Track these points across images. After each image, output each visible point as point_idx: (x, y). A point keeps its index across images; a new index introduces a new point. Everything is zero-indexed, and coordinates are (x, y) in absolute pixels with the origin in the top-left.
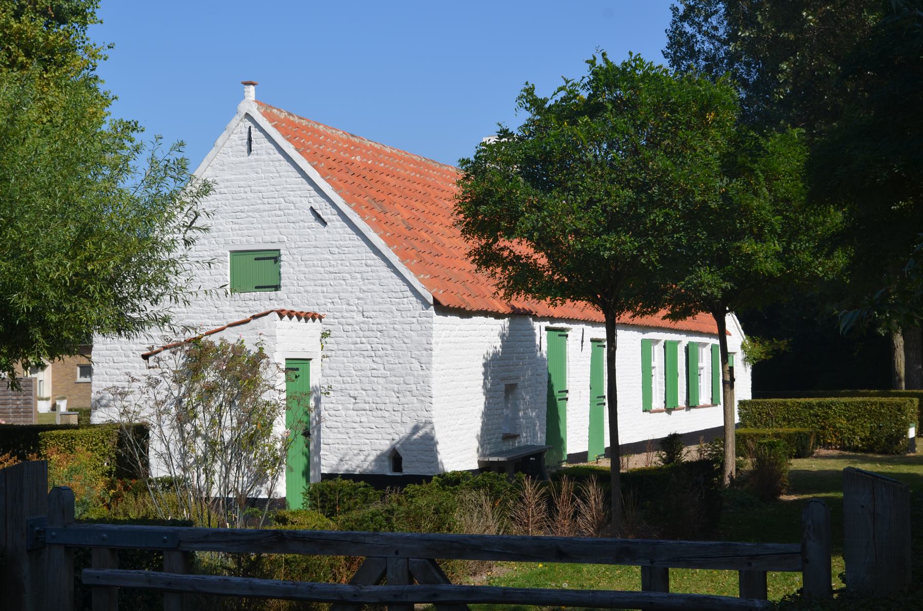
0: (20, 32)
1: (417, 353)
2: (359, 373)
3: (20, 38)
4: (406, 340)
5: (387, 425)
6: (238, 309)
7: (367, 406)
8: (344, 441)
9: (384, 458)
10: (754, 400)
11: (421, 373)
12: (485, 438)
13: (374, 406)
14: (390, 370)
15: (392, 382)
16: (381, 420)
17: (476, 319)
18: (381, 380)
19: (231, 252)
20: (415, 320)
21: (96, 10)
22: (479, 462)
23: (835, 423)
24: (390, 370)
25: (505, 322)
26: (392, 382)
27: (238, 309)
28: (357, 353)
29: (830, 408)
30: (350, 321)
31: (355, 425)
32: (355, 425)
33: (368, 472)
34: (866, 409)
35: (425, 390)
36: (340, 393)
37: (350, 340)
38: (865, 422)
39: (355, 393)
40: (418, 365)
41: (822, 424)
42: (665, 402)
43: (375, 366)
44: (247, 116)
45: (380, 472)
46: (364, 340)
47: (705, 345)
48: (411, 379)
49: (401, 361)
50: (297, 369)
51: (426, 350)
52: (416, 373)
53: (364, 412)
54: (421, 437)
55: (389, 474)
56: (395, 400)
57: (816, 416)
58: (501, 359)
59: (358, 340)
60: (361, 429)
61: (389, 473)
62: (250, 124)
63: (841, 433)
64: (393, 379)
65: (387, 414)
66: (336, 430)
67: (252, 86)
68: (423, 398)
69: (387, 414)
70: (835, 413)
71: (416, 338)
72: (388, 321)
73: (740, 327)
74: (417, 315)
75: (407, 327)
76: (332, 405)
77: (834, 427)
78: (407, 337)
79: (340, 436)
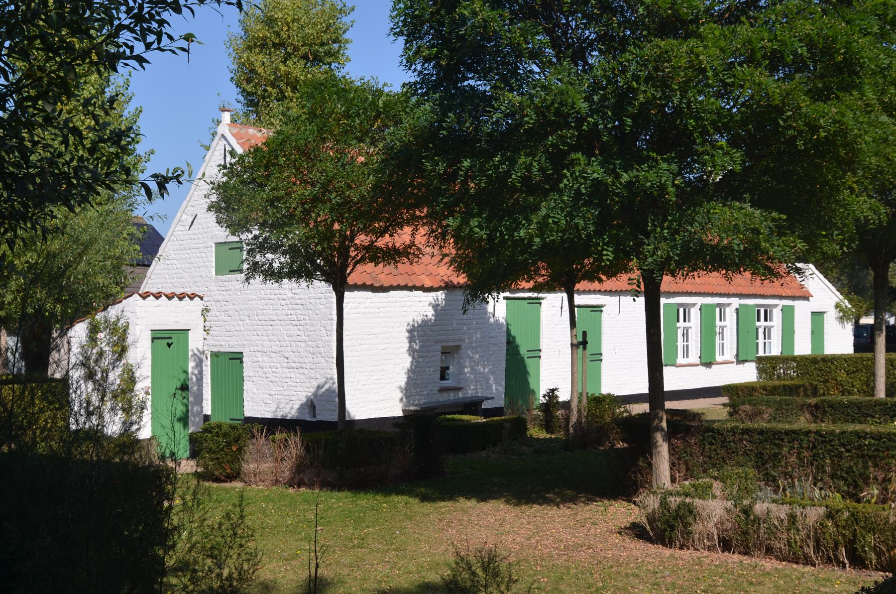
0: (287, 74)
1: (324, 322)
2: (289, 339)
3: (288, 78)
4: (317, 312)
5: (307, 380)
6: (219, 288)
7: (294, 365)
8: (280, 393)
9: (305, 407)
10: (859, 355)
11: (327, 338)
12: (409, 390)
13: (298, 364)
14: (308, 336)
15: (309, 346)
16: (302, 376)
17: (392, 293)
18: (303, 344)
19: (216, 244)
20: (322, 296)
21: (345, 51)
22: (403, 411)
23: (836, 376)
24: (308, 336)
25: (441, 295)
26: (309, 346)
27: (219, 288)
28: (288, 322)
29: (832, 363)
30: (284, 297)
31: (287, 380)
32: (287, 380)
33: (295, 418)
34: (863, 364)
35: (329, 352)
36: (278, 355)
37: (284, 312)
38: (862, 376)
39: (286, 354)
40: (324, 332)
41: (826, 377)
42: (700, 357)
43: (299, 333)
44: (223, 136)
45: (302, 418)
46: (293, 312)
47: (776, 306)
48: (320, 343)
49: (314, 329)
50: (170, 338)
51: (329, 320)
52: (323, 338)
53: (292, 370)
54: (327, 390)
55: (309, 419)
56: (311, 360)
57: (820, 370)
58: (434, 325)
59: (289, 312)
60: (291, 383)
61: (308, 418)
62: (225, 142)
63: (842, 385)
64: (310, 343)
65: (306, 372)
66: (276, 384)
67: (226, 113)
68: (328, 359)
69: (306, 372)
70: (837, 368)
71: (323, 310)
72: (306, 296)
73: (834, 289)
74: (324, 292)
75: (318, 301)
76: (274, 364)
77: (836, 380)
78: (317, 310)
79: (279, 389)
